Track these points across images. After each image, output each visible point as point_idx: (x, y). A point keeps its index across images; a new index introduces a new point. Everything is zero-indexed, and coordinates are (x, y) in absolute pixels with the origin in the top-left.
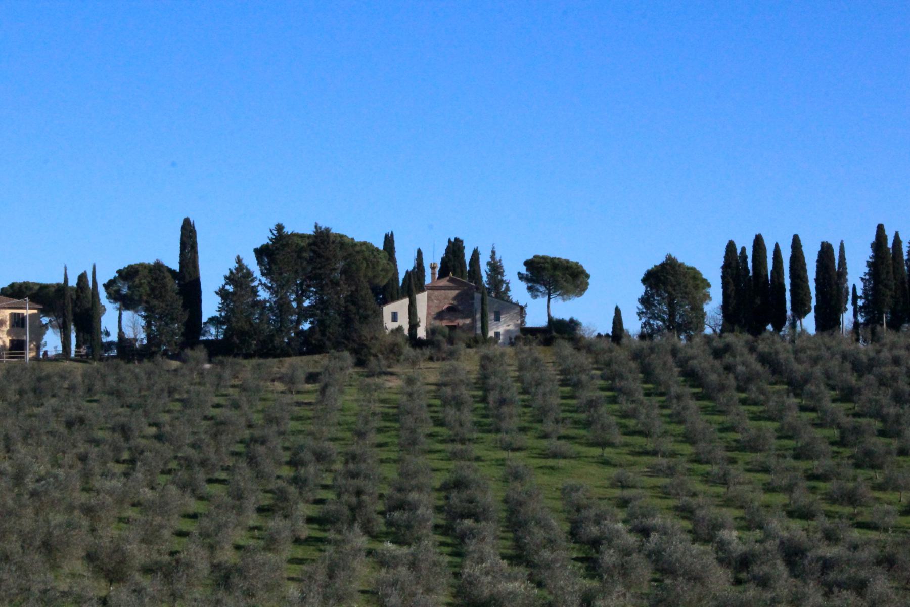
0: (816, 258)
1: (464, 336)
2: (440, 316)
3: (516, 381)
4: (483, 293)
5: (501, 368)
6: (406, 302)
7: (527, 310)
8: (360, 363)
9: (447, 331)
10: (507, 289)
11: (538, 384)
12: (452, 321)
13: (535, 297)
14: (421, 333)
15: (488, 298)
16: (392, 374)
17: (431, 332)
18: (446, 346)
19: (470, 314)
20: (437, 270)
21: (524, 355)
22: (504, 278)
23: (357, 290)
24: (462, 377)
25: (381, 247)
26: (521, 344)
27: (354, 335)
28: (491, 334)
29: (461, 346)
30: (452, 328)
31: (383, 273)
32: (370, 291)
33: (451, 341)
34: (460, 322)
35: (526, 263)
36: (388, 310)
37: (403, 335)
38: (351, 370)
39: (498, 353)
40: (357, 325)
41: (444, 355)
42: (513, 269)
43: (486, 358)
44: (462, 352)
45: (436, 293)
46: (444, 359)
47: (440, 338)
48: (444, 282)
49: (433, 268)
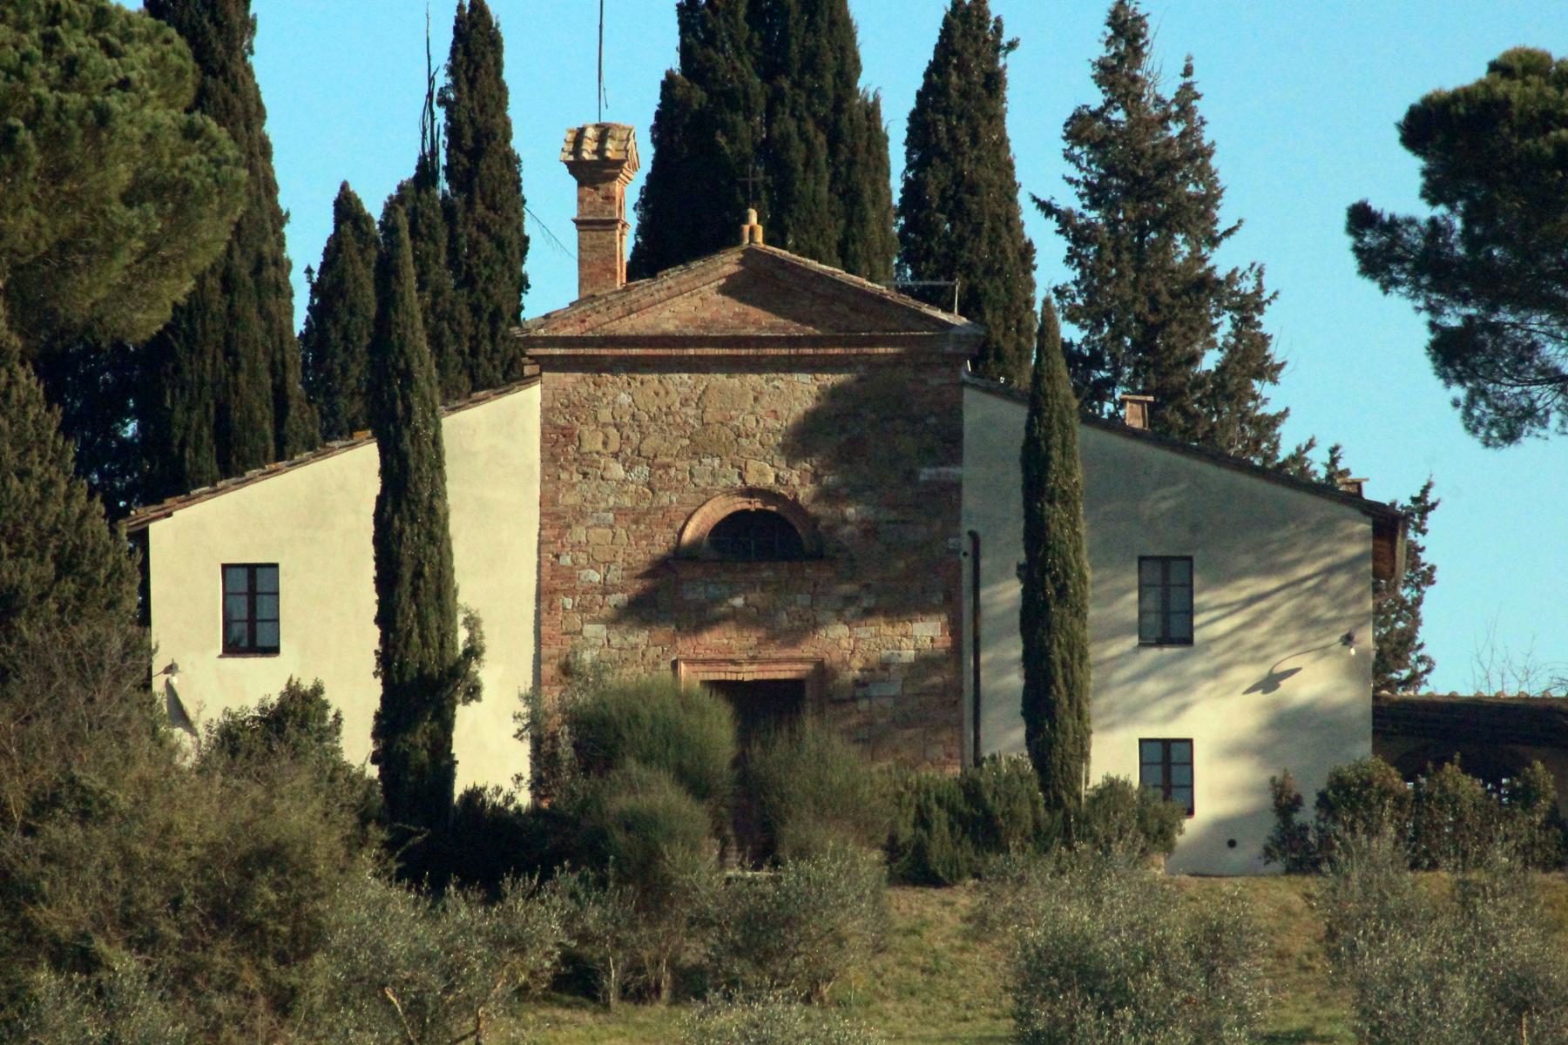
0: (651, 121)
1: (876, 776)
2: (669, 591)
4: (1036, 401)
6: (355, 470)
7: (1436, 542)
9: (719, 730)
10: (1250, 358)
14: (491, 753)
15: (1084, 436)
17: (584, 737)
18: (710, 871)
19: (942, 584)
20: (630, 189)
22: (1221, 261)
26: (1384, 845)
28: (1112, 757)
30: (763, 706)
31: (149, 218)
33: (757, 828)
34: (847, 644)
35: (1426, 126)
37: (335, 773)
39: (1176, 928)
41: (694, 952)
47: (662, 795)
48: (694, 299)
49: (592, 170)
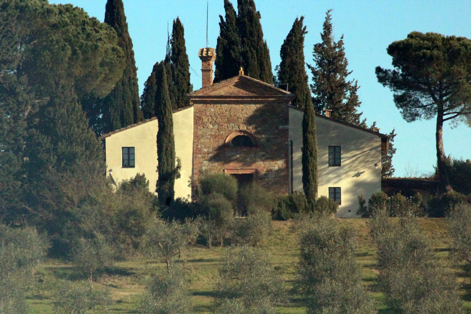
0: (157, 134)
2: (222, 154)
3: (373, 288)
4: (306, 111)
5: (343, 262)
6: (152, 126)
7: (396, 143)
8: (58, 251)
9: (234, 184)
10: (354, 101)
11: (419, 295)
12: (247, 164)
13: (412, 117)
14: (182, 190)
15: (316, 119)
16: (123, 273)
17: (203, 187)
18: (232, 217)
19: (284, 152)
21: (391, 235)
23: (51, 103)
24: (267, 280)
25: (101, 18)
26: (384, 211)
27: (47, 193)
28: (323, 191)
29: (262, 216)
30: (244, 179)
32: (79, 106)
33: (242, 206)
34: (262, 166)
35: (394, 49)
36: (115, 143)
37: (148, 194)
38: (41, 266)
40: (51, 173)
41: (228, 235)
42: (365, 61)
43: (311, 240)
44: (265, 229)
45: (212, 109)
46: (227, 242)
48: (228, 87)
